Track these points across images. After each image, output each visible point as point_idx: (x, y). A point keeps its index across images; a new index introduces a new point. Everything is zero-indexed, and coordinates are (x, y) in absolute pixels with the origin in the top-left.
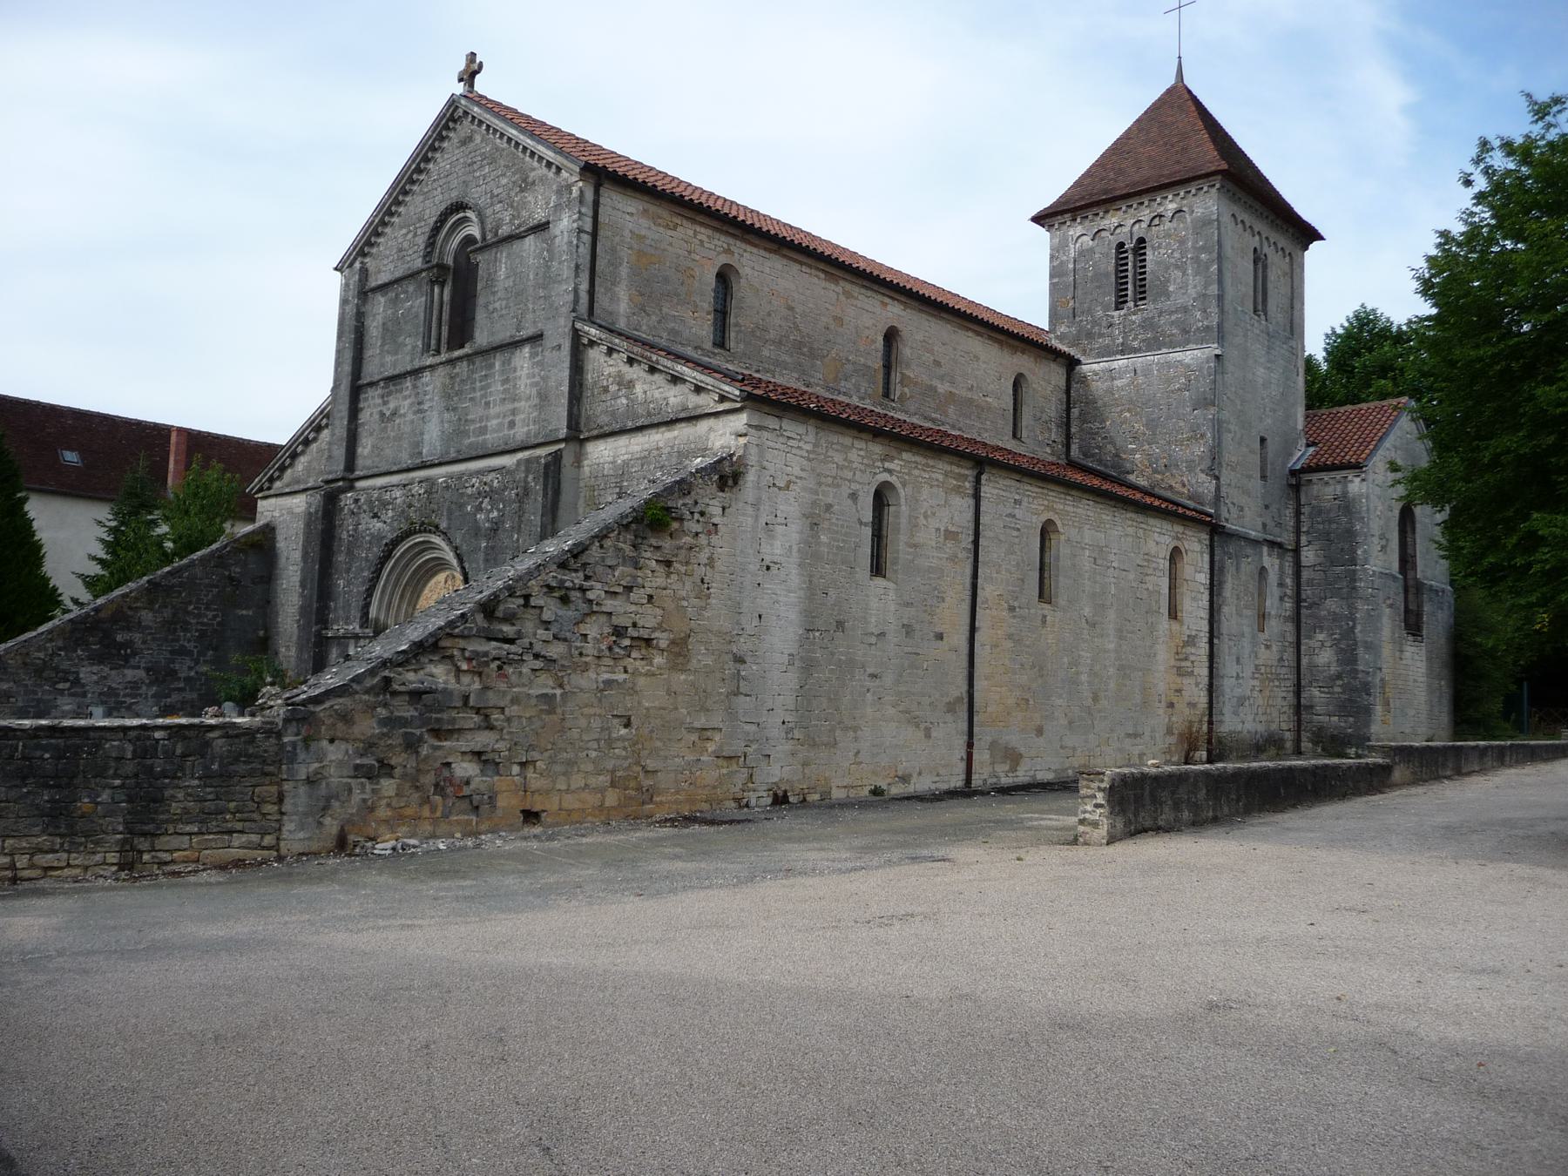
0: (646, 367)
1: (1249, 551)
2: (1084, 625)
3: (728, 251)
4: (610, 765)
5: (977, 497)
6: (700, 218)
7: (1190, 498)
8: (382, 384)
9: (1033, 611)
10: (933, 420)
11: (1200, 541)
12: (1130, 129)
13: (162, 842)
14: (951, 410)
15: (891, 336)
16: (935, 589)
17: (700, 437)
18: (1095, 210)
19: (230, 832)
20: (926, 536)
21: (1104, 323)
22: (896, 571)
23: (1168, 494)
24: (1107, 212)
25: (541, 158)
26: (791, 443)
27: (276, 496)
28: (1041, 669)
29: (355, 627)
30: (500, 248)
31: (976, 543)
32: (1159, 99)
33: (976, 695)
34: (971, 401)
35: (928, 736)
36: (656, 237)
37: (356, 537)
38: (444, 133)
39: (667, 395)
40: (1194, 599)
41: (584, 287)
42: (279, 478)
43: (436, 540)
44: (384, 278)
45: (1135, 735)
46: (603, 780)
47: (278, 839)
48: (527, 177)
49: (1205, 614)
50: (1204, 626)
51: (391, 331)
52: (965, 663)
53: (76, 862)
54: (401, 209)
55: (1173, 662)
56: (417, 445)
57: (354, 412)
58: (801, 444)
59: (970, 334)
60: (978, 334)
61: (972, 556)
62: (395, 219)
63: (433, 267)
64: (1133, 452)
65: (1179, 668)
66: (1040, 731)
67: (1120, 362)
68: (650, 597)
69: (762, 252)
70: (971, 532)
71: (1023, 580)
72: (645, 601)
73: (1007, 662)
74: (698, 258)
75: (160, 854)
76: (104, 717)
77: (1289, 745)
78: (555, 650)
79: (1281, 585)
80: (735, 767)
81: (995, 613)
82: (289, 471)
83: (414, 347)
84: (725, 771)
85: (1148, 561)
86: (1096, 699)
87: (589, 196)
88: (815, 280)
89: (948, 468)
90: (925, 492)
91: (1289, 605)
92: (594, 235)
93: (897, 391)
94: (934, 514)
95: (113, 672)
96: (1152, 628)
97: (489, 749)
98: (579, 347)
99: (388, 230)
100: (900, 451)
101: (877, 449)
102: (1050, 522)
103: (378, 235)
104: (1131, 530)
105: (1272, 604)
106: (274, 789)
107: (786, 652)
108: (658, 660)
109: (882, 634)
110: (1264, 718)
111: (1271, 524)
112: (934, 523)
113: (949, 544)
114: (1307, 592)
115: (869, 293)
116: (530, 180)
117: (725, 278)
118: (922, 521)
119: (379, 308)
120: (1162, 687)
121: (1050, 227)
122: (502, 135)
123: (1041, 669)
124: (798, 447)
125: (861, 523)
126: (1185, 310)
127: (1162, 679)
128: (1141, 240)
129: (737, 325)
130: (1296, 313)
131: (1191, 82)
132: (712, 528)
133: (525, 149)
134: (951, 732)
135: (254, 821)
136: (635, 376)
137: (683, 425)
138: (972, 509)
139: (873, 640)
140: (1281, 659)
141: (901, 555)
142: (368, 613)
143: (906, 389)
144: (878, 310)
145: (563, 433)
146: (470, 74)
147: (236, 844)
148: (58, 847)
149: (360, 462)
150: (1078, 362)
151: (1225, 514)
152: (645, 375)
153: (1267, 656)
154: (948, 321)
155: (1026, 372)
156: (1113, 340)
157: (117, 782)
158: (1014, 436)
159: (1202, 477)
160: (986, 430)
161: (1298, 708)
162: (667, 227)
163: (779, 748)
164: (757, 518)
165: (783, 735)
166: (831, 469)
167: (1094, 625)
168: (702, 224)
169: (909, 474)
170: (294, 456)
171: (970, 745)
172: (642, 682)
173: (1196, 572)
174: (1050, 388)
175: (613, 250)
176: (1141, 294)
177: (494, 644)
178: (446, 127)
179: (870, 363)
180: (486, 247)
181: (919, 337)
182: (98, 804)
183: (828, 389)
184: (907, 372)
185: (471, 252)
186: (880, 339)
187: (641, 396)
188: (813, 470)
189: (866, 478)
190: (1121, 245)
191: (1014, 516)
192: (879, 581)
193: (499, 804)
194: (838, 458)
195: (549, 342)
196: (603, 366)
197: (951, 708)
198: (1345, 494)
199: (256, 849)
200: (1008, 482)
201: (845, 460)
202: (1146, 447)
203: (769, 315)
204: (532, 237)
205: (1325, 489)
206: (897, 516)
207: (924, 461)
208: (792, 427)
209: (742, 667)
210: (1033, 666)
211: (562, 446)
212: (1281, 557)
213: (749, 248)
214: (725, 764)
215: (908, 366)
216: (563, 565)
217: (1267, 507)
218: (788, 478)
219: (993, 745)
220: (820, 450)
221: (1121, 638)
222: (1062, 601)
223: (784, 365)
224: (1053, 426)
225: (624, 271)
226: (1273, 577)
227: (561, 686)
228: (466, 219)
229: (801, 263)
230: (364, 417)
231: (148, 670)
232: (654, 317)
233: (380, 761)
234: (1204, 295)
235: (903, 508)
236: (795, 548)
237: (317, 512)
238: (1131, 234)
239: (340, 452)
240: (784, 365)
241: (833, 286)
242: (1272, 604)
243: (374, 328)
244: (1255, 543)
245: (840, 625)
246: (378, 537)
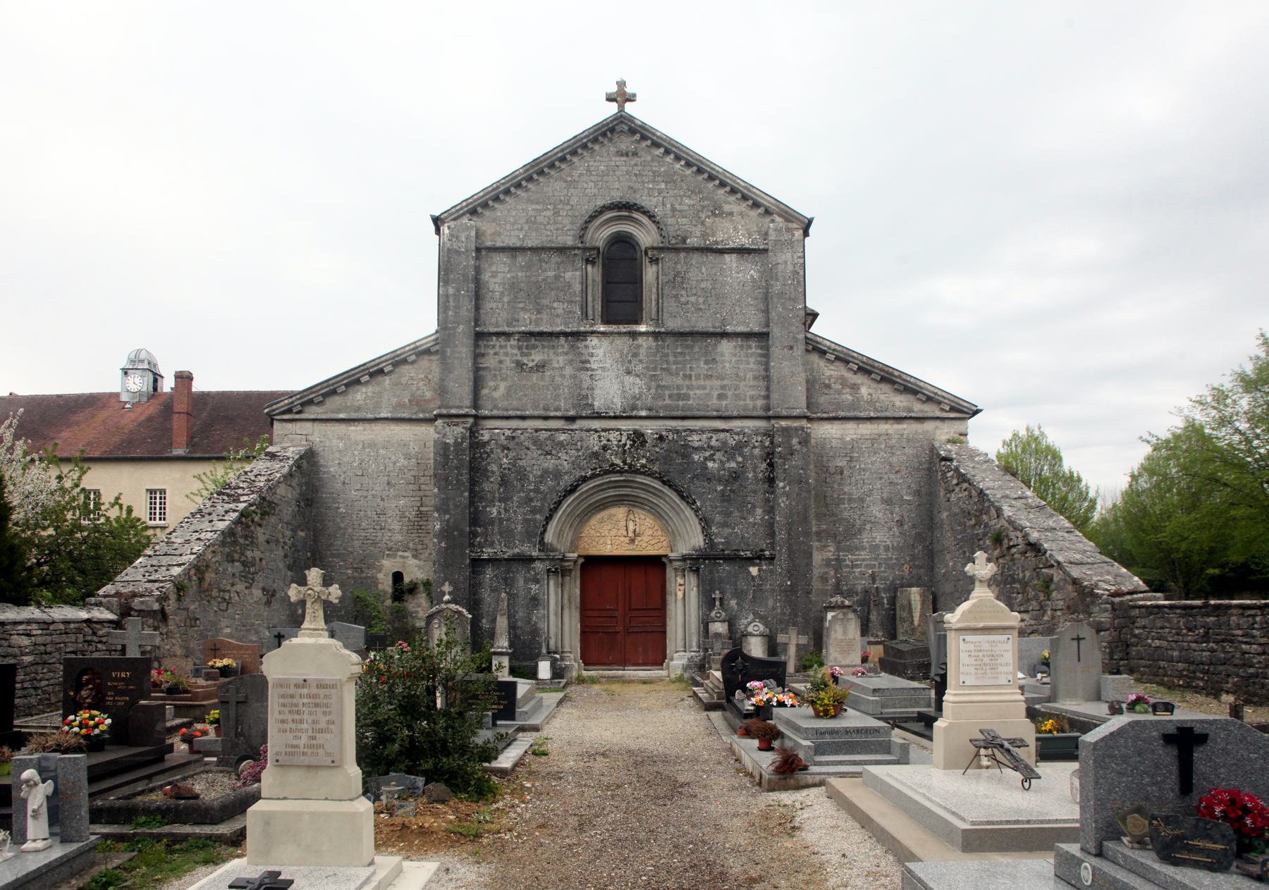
17: (927, 432)
30: (691, 254)
76: (1087, 700)
136: (859, 382)
137: (912, 421)
178: (604, 135)
199: (54, 751)
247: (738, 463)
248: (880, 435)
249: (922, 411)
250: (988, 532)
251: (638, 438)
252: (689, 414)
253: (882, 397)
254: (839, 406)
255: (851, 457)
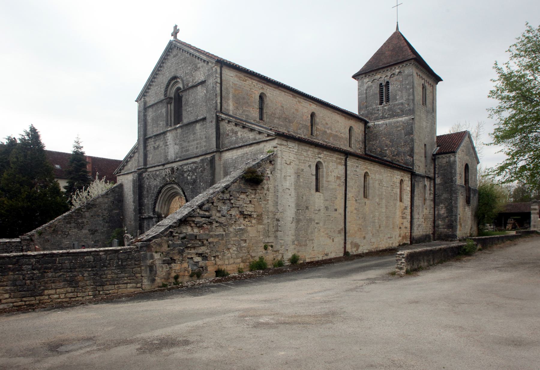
0: (242, 127)
1: (421, 180)
2: (377, 205)
3: (262, 88)
4: (241, 255)
5: (346, 165)
6: (254, 78)
7: (404, 164)
8: (153, 137)
9: (362, 201)
10: (326, 142)
11: (408, 177)
12: (382, 46)
13: (106, 287)
14: (331, 139)
15: (313, 115)
16: (334, 195)
17: (261, 149)
18: (373, 73)
19: (127, 283)
20: (331, 178)
21: (376, 109)
22: (323, 190)
23: (397, 163)
24: (376, 73)
25: (201, 59)
26: (291, 149)
27: (122, 175)
28: (365, 219)
29: (151, 214)
31: (346, 180)
32: (391, 36)
33: (347, 227)
34: (337, 136)
35: (333, 241)
36: (240, 84)
37: (150, 186)
38: (168, 53)
39: (249, 135)
40: (407, 195)
41: (219, 101)
42: (123, 169)
43: (175, 186)
44: (152, 103)
45: (391, 238)
46: (239, 260)
47: (142, 285)
48: (197, 66)
49: (409, 200)
50: (409, 203)
51: (155, 120)
52: (343, 218)
53: (79, 295)
54: (155, 80)
55: (401, 215)
56: (166, 156)
57: (145, 147)
58: (294, 150)
59: (336, 114)
60: (338, 114)
61: (344, 184)
62: (154, 84)
63: (167, 98)
64: (386, 150)
65: (403, 217)
66: (364, 238)
67: (382, 122)
68: (250, 201)
69: (273, 89)
70: (344, 177)
71: (359, 191)
72: (249, 203)
73: (355, 217)
74: (253, 91)
75: (105, 291)
77: (432, 238)
78: (223, 220)
79: (430, 190)
80: (278, 254)
81: (351, 202)
82: (126, 167)
83: (163, 125)
84: (275, 255)
85: (394, 184)
86: (380, 227)
87: (219, 71)
88: (289, 97)
89: (337, 156)
90: (331, 164)
91: (432, 196)
92: (221, 84)
93: (315, 133)
94: (333, 171)
95: (79, 231)
96: (395, 205)
97: (204, 253)
98: (218, 120)
99: (151, 87)
100: (323, 151)
101: (316, 150)
102: (366, 173)
103: (149, 89)
104: (389, 175)
105: (427, 196)
106: (139, 269)
107: (292, 217)
108: (254, 221)
109: (319, 210)
110: (425, 230)
111: (427, 171)
112: (333, 174)
113: (338, 181)
114: (437, 192)
115: (306, 101)
116: (198, 67)
117: (262, 97)
118: (330, 173)
119: (151, 114)
120: (398, 223)
121: (358, 79)
122: (188, 52)
123: (365, 219)
124: (293, 151)
125: (312, 175)
126: (402, 104)
127: (398, 220)
128: (388, 82)
129: (266, 113)
130: (434, 104)
131: (400, 30)
132: (268, 178)
133: (196, 56)
134: (339, 239)
135: (134, 279)
136: (238, 130)
137: (255, 145)
138: (344, 169)
139: (317, 212)
140: (430, 213)
141: (324, 185)
142: (155, 210)
143: (318, 132)
144: (309, 107)
145: (214, 149)
146: (175, 33)
147: (129, 287)
148: (73, 291)
149: (148, 163)
150: (368, 122)
151: (415, 169)
152: (240, 129)
153: (426, 212)
154: (329, 110)
155: (353, 126)
156: (379, 115)
157: (90, 269)
158: (350, 146)
159: (408, 157)
160: (342, 145)
161: (434, 227)
162: (243, 81)
163: (291, 247)
164: (281, 174)
165: (292, 243)
166: (302, 158)
167: (379, 204)
168: (254, 79)
169: (326, 159)
170: (127, 162)
171: (345, 243)
172: (249, 228)
173: (407, 187)
174: (360, 131)
175: (227, 89)
176: (388, 100)
177: (204, 219)
179: (307, 124)
180: (185, 90)
181: (321, 115)
182: (84, 277)
183: (294, 132)
184: (318, 127)
185: (180, 92)
186: (310, 116)
187: (240, 137)
188: (297, 158)
189: (313, 160)
190: (381, 84)
191: (356, 171)
192: (318, 193)
193: (208, 270)
194: (305, 154)
195: (208, 120)
196: (226, 127)
197: (339, 232)
198: (450, 161)
200: (354, 160)
201: (307, 154)
202: (390, 148)
203: (276, 109)
204: (200, 86)
205: (443, 160)
206: (323, 172)
207: (330, 154)
208: (291, 144)
209: (279, 222)
210: (362, 218)
211: (215, 154)
212: (430, 182)
213: (269, 87)
214: (275, 253)
215: (318, 125)
216: (223, 192)
217: (426, 166)
218: (290, 161)
219: (352, 243)
220: (299, 151)
221: (387, 208)
222: (370, 197)
223: (281, 126)
224: (361, 143)
225: (231, 96)
226: (428, 188)
227: (225, 231)
228: (177, 82)
229: (285, 92)
230: (148, 148)
231: (89, 230)
232: (241, 111)
233: (171, 258)
234: (408, 99)
235: (324, 169)
236: (293, 184)
237: (136, 179)
238: (384, 80)
239: (142, 160)
240: (281, 126)
241: (295, 99)
242: (427, 196)
243: (149, 119)
244: (423, 177)
245: (307, 208)
246: (156, 186)
247: (195, 176)
248: (244, 154)
249: (259, 139)
250: (520, 85)
251: (173, 169)
252: (189, 157)
253: (245, 135)
254: (231, 143)
255: (235, 166)
